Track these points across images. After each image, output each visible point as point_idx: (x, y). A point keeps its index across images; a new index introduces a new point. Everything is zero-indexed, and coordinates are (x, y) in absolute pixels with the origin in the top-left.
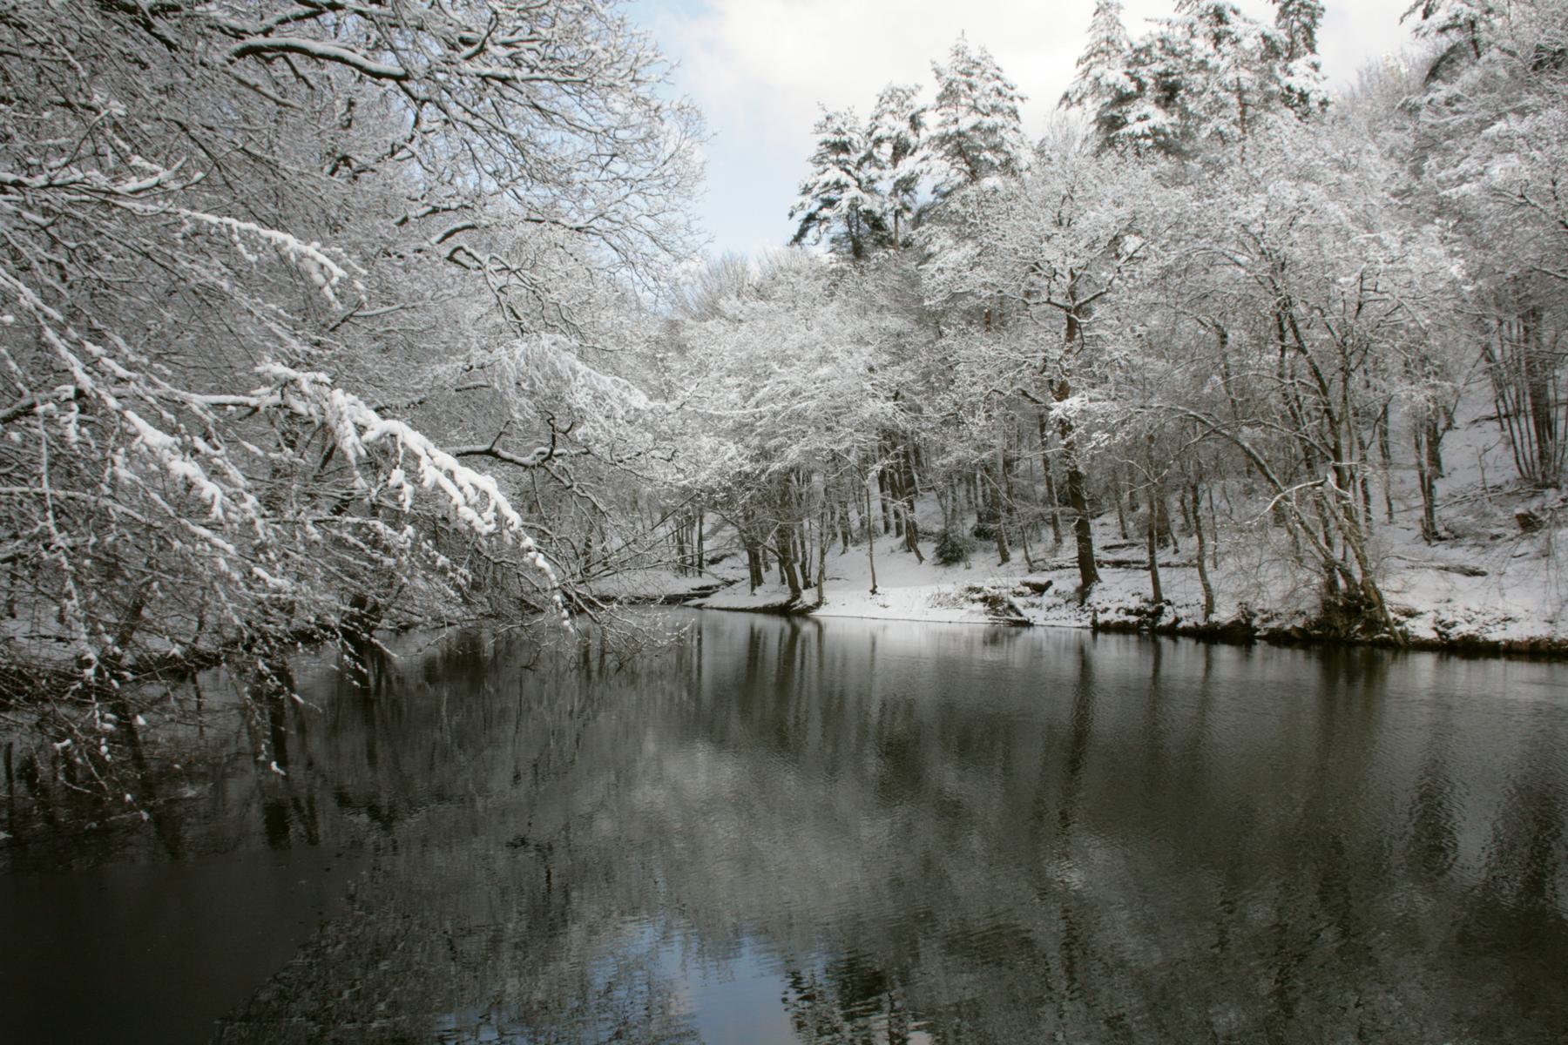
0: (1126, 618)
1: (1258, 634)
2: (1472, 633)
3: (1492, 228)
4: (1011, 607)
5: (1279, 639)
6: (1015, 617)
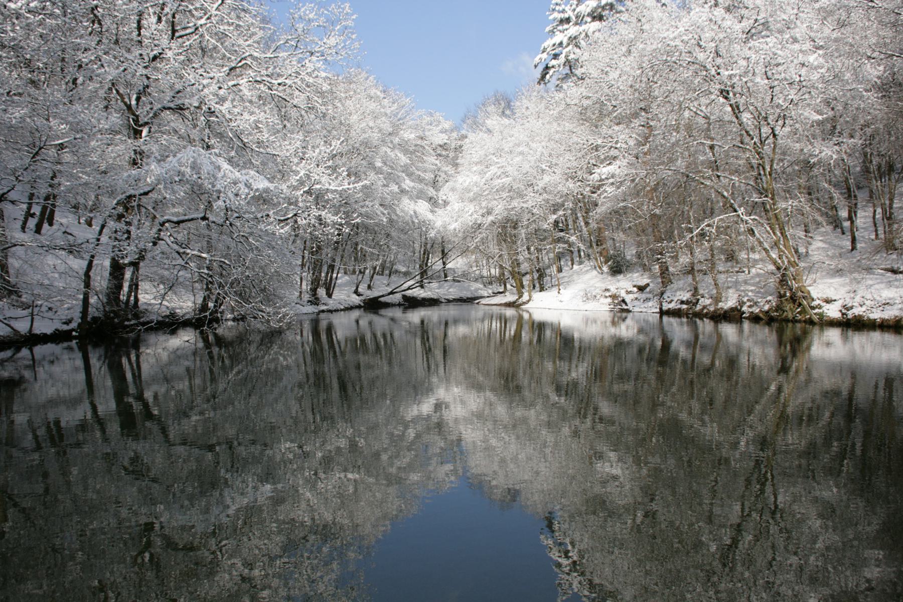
0: (679, 306)
1: (744, 315)
2: (861, 313)
3: (246, 348)
4: (623, 301)
5: (755, 319)
6: (625, 307)
